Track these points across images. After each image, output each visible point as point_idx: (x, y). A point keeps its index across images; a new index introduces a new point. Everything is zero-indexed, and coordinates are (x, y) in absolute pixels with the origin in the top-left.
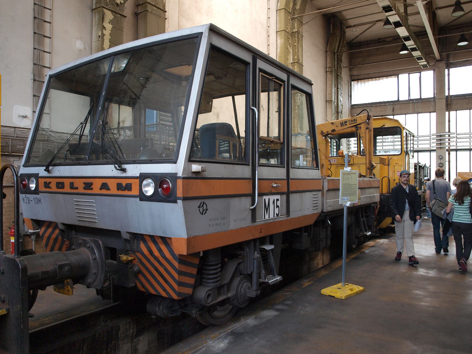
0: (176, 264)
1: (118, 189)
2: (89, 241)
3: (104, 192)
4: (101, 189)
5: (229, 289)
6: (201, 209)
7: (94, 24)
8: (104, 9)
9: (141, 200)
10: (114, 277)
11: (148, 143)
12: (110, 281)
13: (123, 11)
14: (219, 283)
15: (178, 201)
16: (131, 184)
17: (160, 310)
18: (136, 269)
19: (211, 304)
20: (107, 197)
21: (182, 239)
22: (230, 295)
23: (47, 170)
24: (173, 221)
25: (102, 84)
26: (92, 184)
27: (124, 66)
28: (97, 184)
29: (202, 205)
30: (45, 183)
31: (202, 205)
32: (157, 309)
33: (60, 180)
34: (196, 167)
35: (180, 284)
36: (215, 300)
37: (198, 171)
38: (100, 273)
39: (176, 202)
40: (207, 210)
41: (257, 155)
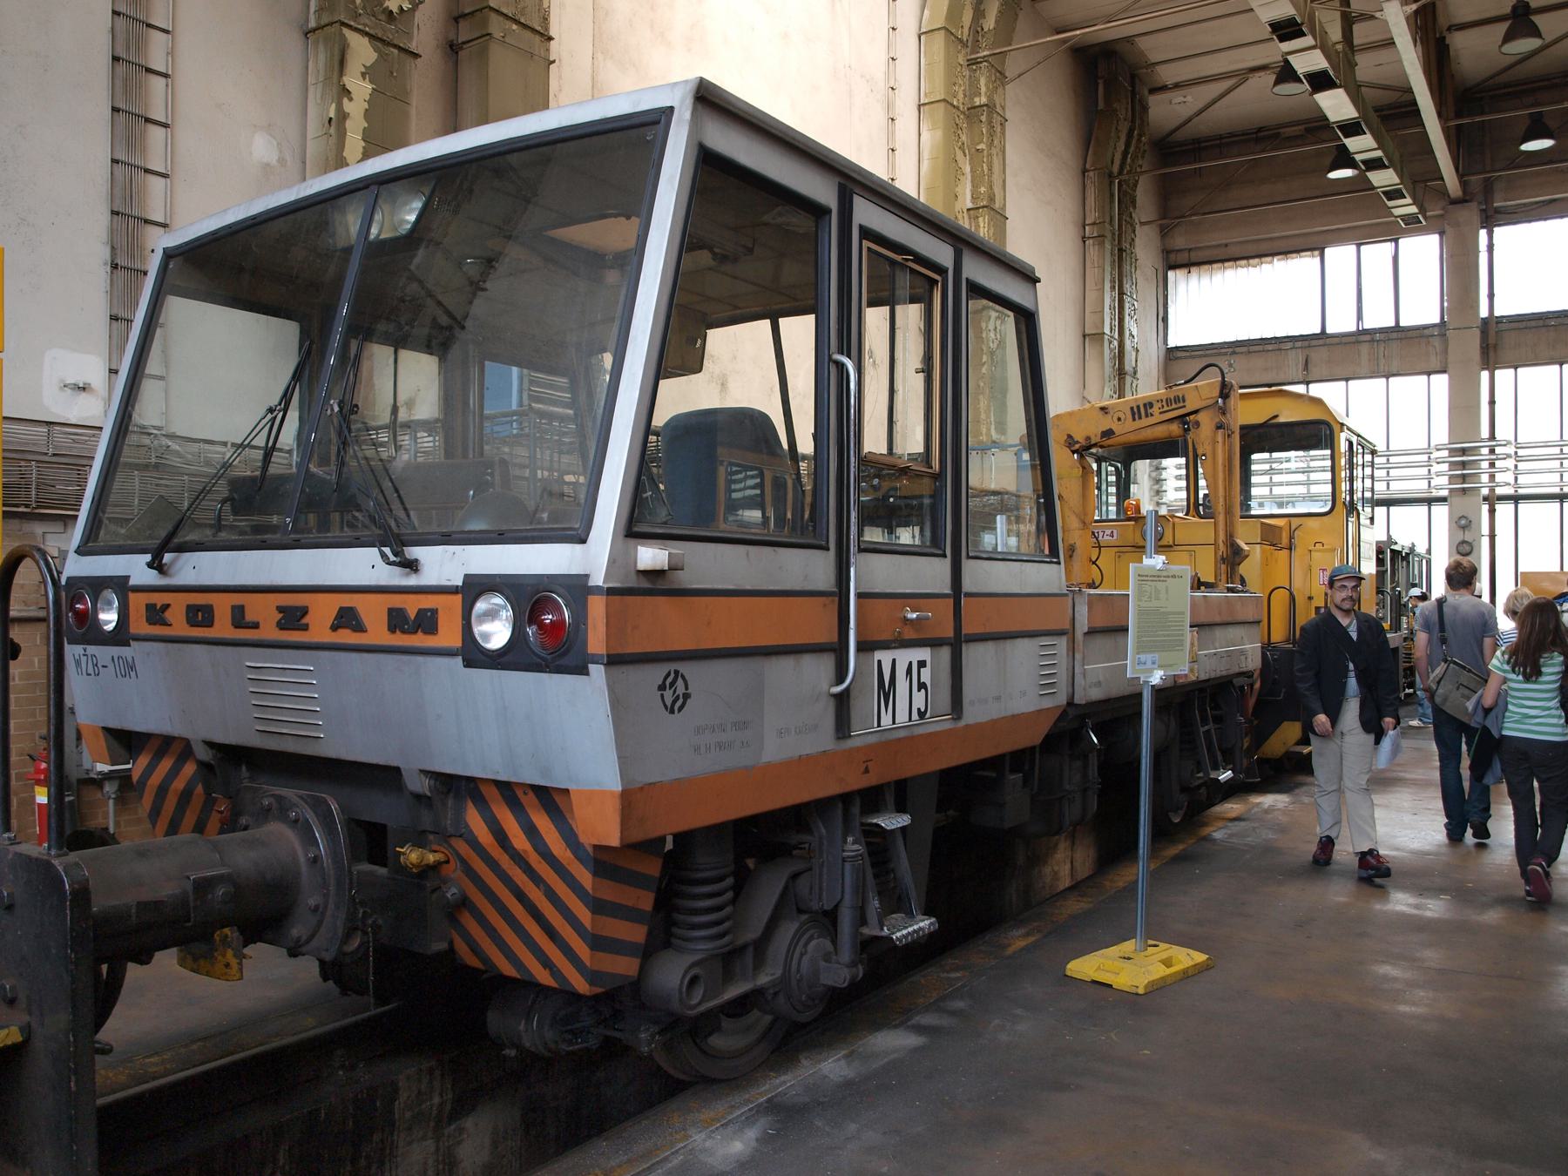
0: (585, 878)
1: (392, 629)
2: (296, 800)
3: (346, 637)
4: (334, 628)
5: (760, 961)
6: (668, 695)
7: (311, 80)
8: (346, 31)
9: (468, 664)
10: (380, 922)
11: (492, 475)
12: (365, 933)
13: (409, 35)
14: (727, 939)
15: (591, 667)
16: (434, 612)
17: (530, 1031)
18: (451, 892)
19: (702, 1008)
20: (354, 656)
21: (603, 792)
22: (763, 979)
23: (157, 565)
24: (573, 735)
25: (340, 279)
26: (304, 611)
27: (412, 218)
28: (322, 612)
29: (670, 680)
30: (150, 608)
31: (670, 680)
32: (522, 1027)
33: (200, 599)
34: (650, 556)
35: (599, 943)
36: (715, 997)
37: (658, 568)
38: (331, 906)
39: (583, 671)
40: (686, 696)
41: (853, 515)
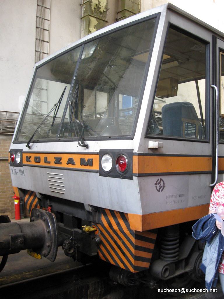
0: (133, 239)
1: (82, 164)
2: (45, 214)
3: (70, 166)
4: (68, 164)
5: (187, 264)
6: (158, 186)
7: (82, 29)
8: (90, 17)
9: (101, 175)
10: (79, 245)
11: (113, 122)
12: (75, 248)
13: (105, 17)
14: (177, 258)
15: (134, 177)
16: (92, 160)
17: (121, 279)
18: (97, 239)
19: (169, 278)
20: (72, 172)
21: (137, 215)
22: (188, 269)
23: (28, 146)
24: (128, 197)
25: (74, 71)
26: (61, 159)
27: (92, 52)
28: (65, 159)
29: (159, 181)
30: (27, 157)
31: (159, 181)
32: (118, 277)
33: (37, 155)
34: (153, 144)
35: (136, 258)
36: (172, 275)
37: (155, 147)
38: (53, 246)
39: (131, 178)
40: (164, 187)
41: (217, 133)
